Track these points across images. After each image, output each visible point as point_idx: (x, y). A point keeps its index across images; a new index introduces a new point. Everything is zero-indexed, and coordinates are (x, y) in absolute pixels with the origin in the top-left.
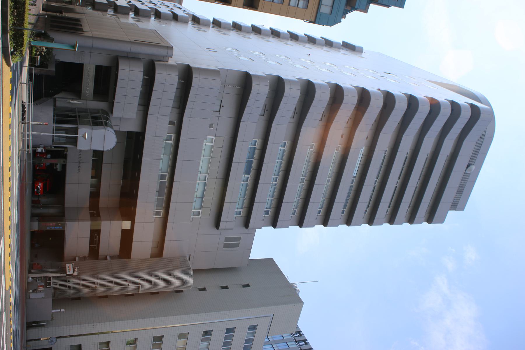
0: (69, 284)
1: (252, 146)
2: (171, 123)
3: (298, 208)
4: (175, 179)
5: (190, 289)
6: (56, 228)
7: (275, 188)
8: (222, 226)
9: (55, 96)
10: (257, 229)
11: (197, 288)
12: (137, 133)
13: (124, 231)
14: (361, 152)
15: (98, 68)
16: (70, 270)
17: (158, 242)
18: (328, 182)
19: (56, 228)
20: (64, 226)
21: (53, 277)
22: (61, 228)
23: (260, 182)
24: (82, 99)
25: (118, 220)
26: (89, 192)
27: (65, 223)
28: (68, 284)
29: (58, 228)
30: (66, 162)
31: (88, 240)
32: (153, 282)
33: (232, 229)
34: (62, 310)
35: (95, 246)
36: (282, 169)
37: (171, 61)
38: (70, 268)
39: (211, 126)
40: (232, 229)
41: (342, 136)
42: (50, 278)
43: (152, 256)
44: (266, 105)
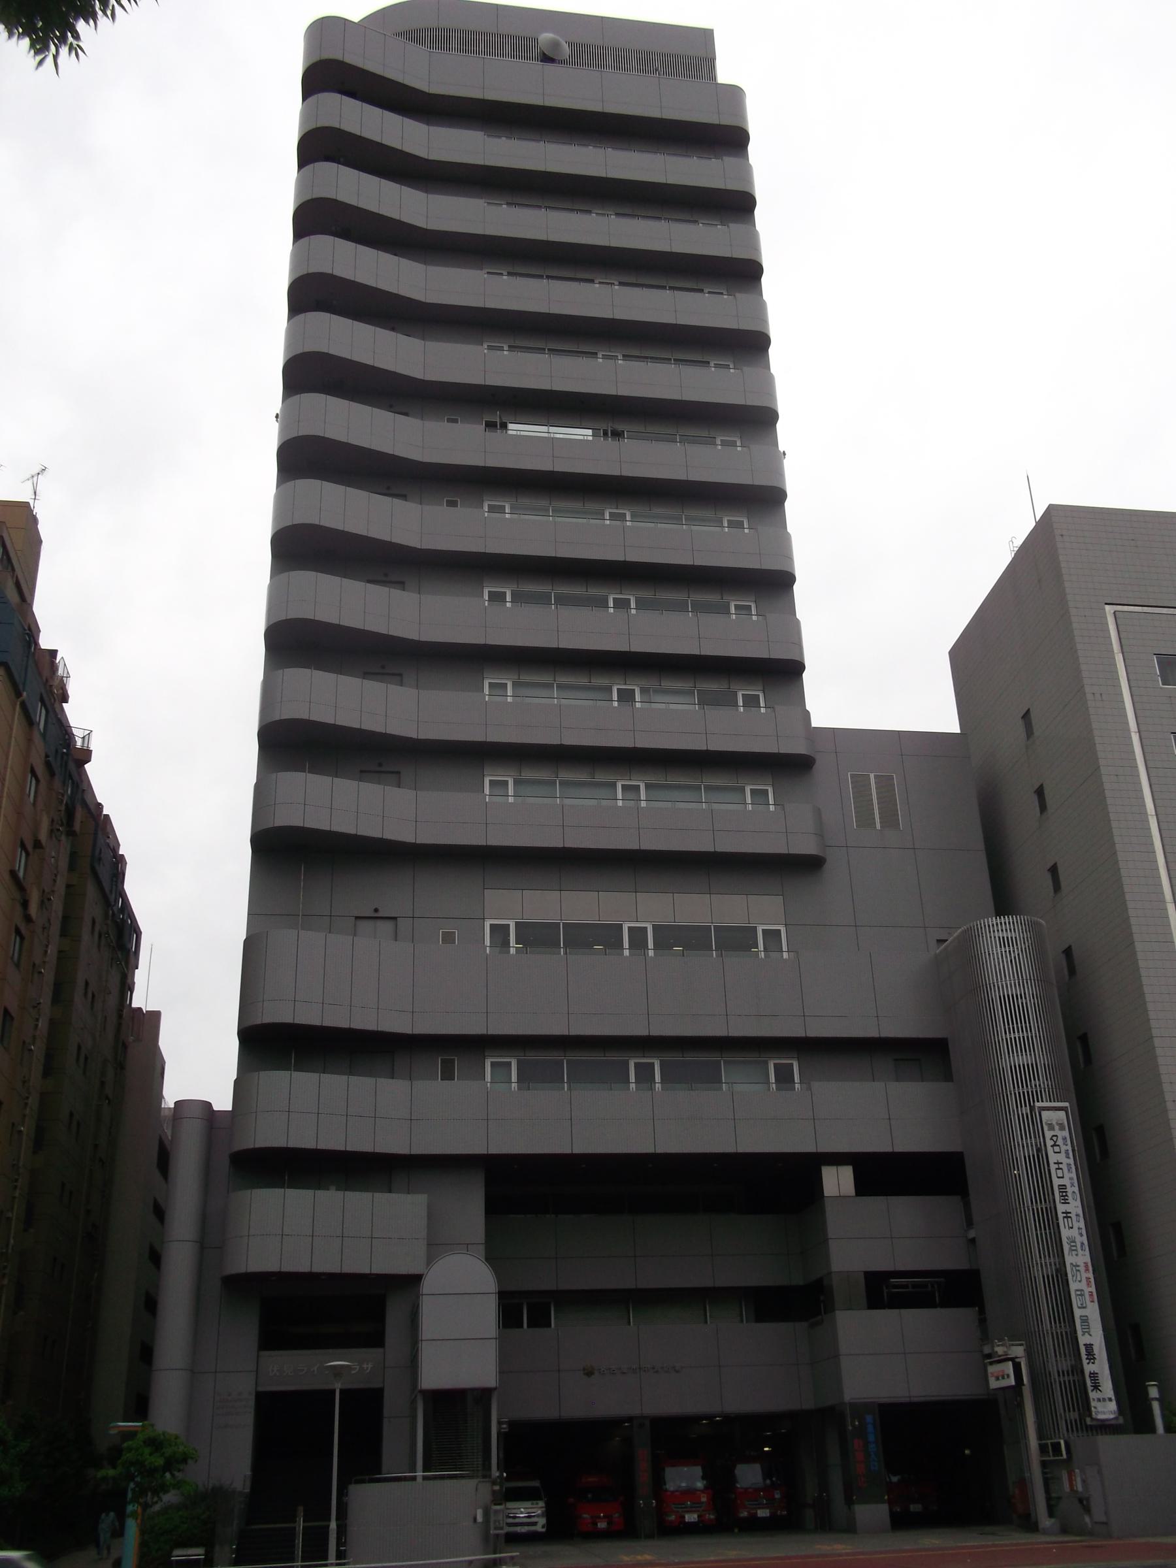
0: (1058, 1372)
1: (771, 801)
2: (448, 1075)
3: (726, 598)
4: (641, 1031)
5: (1043, 922)
6: (871, 1438)
7: (655, 691)
8: (805, 846)
9: (128, 1500)
10: (816, 722)
11: (1054, 897)
12: (488, 1185)
13: (864, 1187)
14: (546, 435)
15: (271, 1340)
16: (1003, 1371)
17: (896, 1060)
18: (622, 517)
19: (871, 1438)
20: (859, 1409)
21: (1041, 1436)
22: (869, 1418)
23: (478, 737)
24: (380, 1385)
25: (822, 1211)
26: (759, 1325)
27: (850, 1404)
28: (1059, 1375)
29: (870, 1428)
30: (643, 1417)
31: (911, 1316)
32: (1022, 1059)
33: (818, 813)
34: (1154, 1392)
35: (936, 1286)
36: (726, 686)
37: (223, 1102)
38: (1001, 1377)
39: (448, 938)
40: (818, 813)
41: (452, 504)
42: (1043, 1449)
43: (948, 1077)
44: (362, 772)
